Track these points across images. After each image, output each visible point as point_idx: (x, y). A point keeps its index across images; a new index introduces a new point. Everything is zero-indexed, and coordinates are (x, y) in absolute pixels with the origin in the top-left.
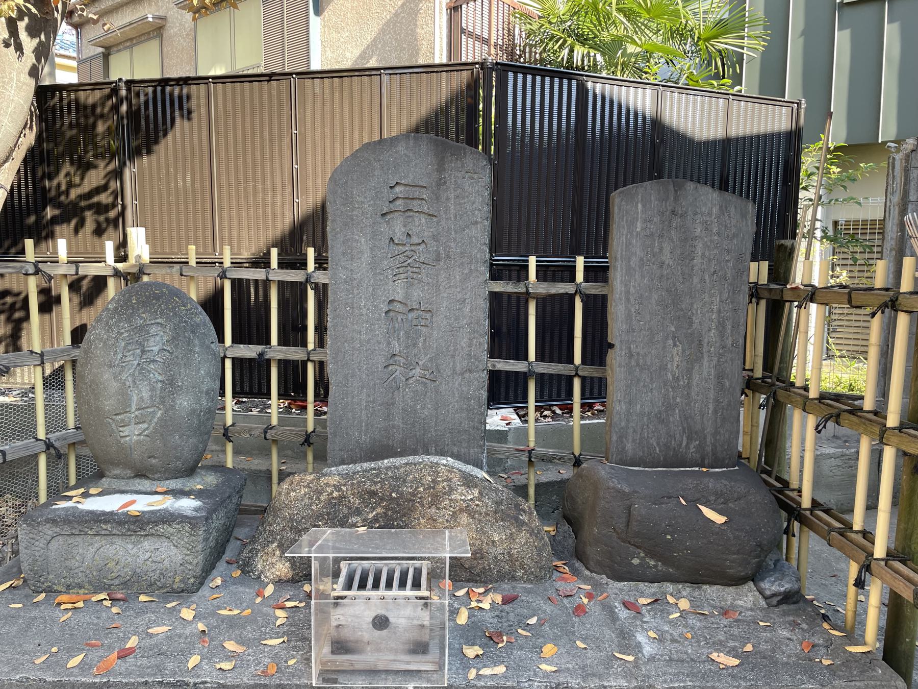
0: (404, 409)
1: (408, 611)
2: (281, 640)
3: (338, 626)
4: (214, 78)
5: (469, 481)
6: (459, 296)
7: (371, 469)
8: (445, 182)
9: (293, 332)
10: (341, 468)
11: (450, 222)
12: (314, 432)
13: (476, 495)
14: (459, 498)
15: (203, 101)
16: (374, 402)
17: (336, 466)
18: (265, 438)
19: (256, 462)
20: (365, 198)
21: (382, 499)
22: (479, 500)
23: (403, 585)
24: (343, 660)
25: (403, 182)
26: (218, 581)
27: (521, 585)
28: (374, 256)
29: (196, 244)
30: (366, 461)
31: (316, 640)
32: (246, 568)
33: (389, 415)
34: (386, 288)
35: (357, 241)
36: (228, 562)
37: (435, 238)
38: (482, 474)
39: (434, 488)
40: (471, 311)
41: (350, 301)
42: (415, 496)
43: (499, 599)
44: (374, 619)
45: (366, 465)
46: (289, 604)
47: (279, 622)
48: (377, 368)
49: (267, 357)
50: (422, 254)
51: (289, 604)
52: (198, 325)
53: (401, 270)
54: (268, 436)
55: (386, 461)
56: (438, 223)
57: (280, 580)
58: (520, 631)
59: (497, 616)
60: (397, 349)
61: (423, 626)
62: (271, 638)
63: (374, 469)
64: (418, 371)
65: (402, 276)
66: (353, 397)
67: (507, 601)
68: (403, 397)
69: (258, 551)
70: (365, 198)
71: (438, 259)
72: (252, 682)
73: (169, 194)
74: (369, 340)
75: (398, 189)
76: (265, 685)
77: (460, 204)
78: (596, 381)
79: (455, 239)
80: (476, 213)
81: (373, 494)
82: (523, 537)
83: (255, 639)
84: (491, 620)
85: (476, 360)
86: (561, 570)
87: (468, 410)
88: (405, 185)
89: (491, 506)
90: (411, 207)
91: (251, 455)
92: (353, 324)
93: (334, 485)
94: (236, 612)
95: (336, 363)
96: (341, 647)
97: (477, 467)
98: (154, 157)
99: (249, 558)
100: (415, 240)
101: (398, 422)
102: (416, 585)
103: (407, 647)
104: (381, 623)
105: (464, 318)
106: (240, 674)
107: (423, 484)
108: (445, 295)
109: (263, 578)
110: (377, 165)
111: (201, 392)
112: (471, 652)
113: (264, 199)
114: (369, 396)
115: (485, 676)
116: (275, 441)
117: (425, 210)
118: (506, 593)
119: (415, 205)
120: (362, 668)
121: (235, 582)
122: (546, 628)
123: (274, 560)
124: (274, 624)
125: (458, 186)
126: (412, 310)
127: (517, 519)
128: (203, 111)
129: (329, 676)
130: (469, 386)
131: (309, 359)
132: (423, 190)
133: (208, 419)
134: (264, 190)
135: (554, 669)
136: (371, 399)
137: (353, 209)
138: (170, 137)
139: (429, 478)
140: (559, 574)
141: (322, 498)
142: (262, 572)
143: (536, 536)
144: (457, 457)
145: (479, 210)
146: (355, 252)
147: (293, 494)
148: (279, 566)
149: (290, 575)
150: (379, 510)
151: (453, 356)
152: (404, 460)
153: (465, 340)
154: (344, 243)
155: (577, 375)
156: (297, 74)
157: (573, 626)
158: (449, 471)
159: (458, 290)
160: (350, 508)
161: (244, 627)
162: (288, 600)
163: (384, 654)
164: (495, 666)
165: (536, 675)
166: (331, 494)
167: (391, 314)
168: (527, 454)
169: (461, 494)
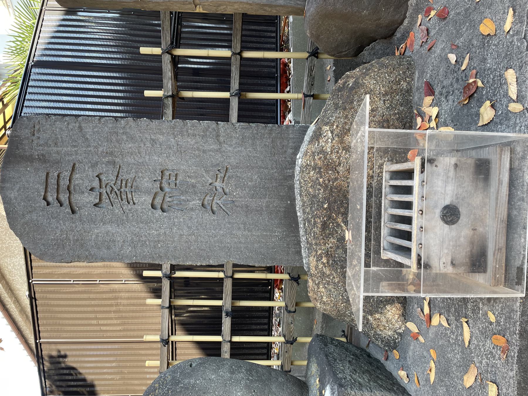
0: (252, 197)
1: (439, 183)
2: (465, 325)
3: (453, 264)
4: (36, 339)
5: (317, 136)
6: (148, 144)
7: (304, 227)
8: (43, 155)
9: (212, 288)
10: (304, 255)
11: (79, 152)
12: (289, 274)
13: (328, 128)
14: (330, 144)
15: (53, 347)
16: (245, 224)
17: (302, 258)
18: (294, 312)
19: (317, 317)
20: (57, 228)
21: (330, 217)
22: (333, 125)
23: (408, 190)
24: (493, 260)
25: (43, 194)
26: (402, 374)
27: (416, 83)
28: (111, 222)
29: (145, 361)
30: (299, 232)
31: (467, 292)
32: (391, 345)
33: (257, 211)
34: (140, 210)
35: (97, 236)
36: (387, 359)
37: (94, 165)
38: (312, 127)
39: (320, 168)
40: (163, 134)
41: (152, 244)
42: (327, 186)
43: (428, 100)
44: (447, 222)
45: (302, 232)
46: (426, 310)
47: (445, 324)
48: (214, 220)
49: (230, 309)
50: (109, 178)
51: (426, 310)
52: (173, 378)
53: (124, 197)
54: (293, 309)
55: (298, 214)
56: (81, 163)
57: (403, 315)
58: (463, 68)
59: (446, 97)
60: (198, 203)
61: (456, 165)
62: (462, 334)
63: (305, 224)
64: (218, 184)
65: (130, 196)
66: (240, 242)
67: (430, 90)
68: (241, 197)
69: (376, 334)
70: (57, 228)
71: (114, 163)
72: (515, 367)
73: (122, 373)
74: (188, 227)
75: (50, 199)
76: (520, 351)
77: (62, 142)
78: (244, 38)
79: (96, 147)
80: (70, 127)
81: (324, 226)
82: (369, 82)
83: (463, 352)
84: (450, 102)
85: (207, 130)
86: (403, 50)
87: (254, 138)
88: (46, 192)
89: (339, 113)
90: (65, 187)
91: (313, 320)
92: (174, 241)
93: (317, 261)
94: (432, 365)
95: (209, 257)
96: (477, 262)
97: (306, 131)
98: (96, 383)
99: (382, 341)
100: (96, 184)
101: (264, 202)
102: (409, 174)
103: (481, 184)
104: (450, 215)
105: (168, 140)
106: (504, 378)
107: (317, 179)
108: (147, 157)
109: (401, 331)
110: (28, 217)
111: (231, 378)
112: (487, 113)
113: (124, 305)
114: (239, 228)
115: (519, 91)
116: (297, 304)
117: (67, 174)
118: (423, 95)
119: (64, 183)
120: (504, 238)
121: (403, 357)
122: (459, 42)
123: (384, 320)
124: (446, 329)
125: (46, 144)
126: (161, 189)
127: (352, 88)
128: (60, 347)
129: (513, 276)
130: (231, 137)
131: (232, 277)
132: (50, 175)
133: (257, 372)
134: (117, 305)
135: (511, 11)
136: (242, 226)
137: (67, 239)
138: (81, 371)
139: (312, 173)
140: (407, 51)
141: (328, 272)
142: (395, 331)
143: (369, 69)
144: (297, 149)
145: (68, 124)
146: (108, 238)
147: (325, 299)
148: (389, 315)
149: (399, 306)
150: (340, 220)
151: (204, 152)
152: (298, 197)
153: (189, 140)
154: (99, 248)
155: (240, 54)
156: (29, 279)
157: (459, 14)
158: (306, 155)
159: (142, 145)
160: (338, 247)
161: (449, 361)
162: (422, 310)
163: (486, 212)
164: (506, 83)
165: (518, 33)
166: (324, 264)
167: (165, 207)
168: (307, 99)
169: (327, 142)
